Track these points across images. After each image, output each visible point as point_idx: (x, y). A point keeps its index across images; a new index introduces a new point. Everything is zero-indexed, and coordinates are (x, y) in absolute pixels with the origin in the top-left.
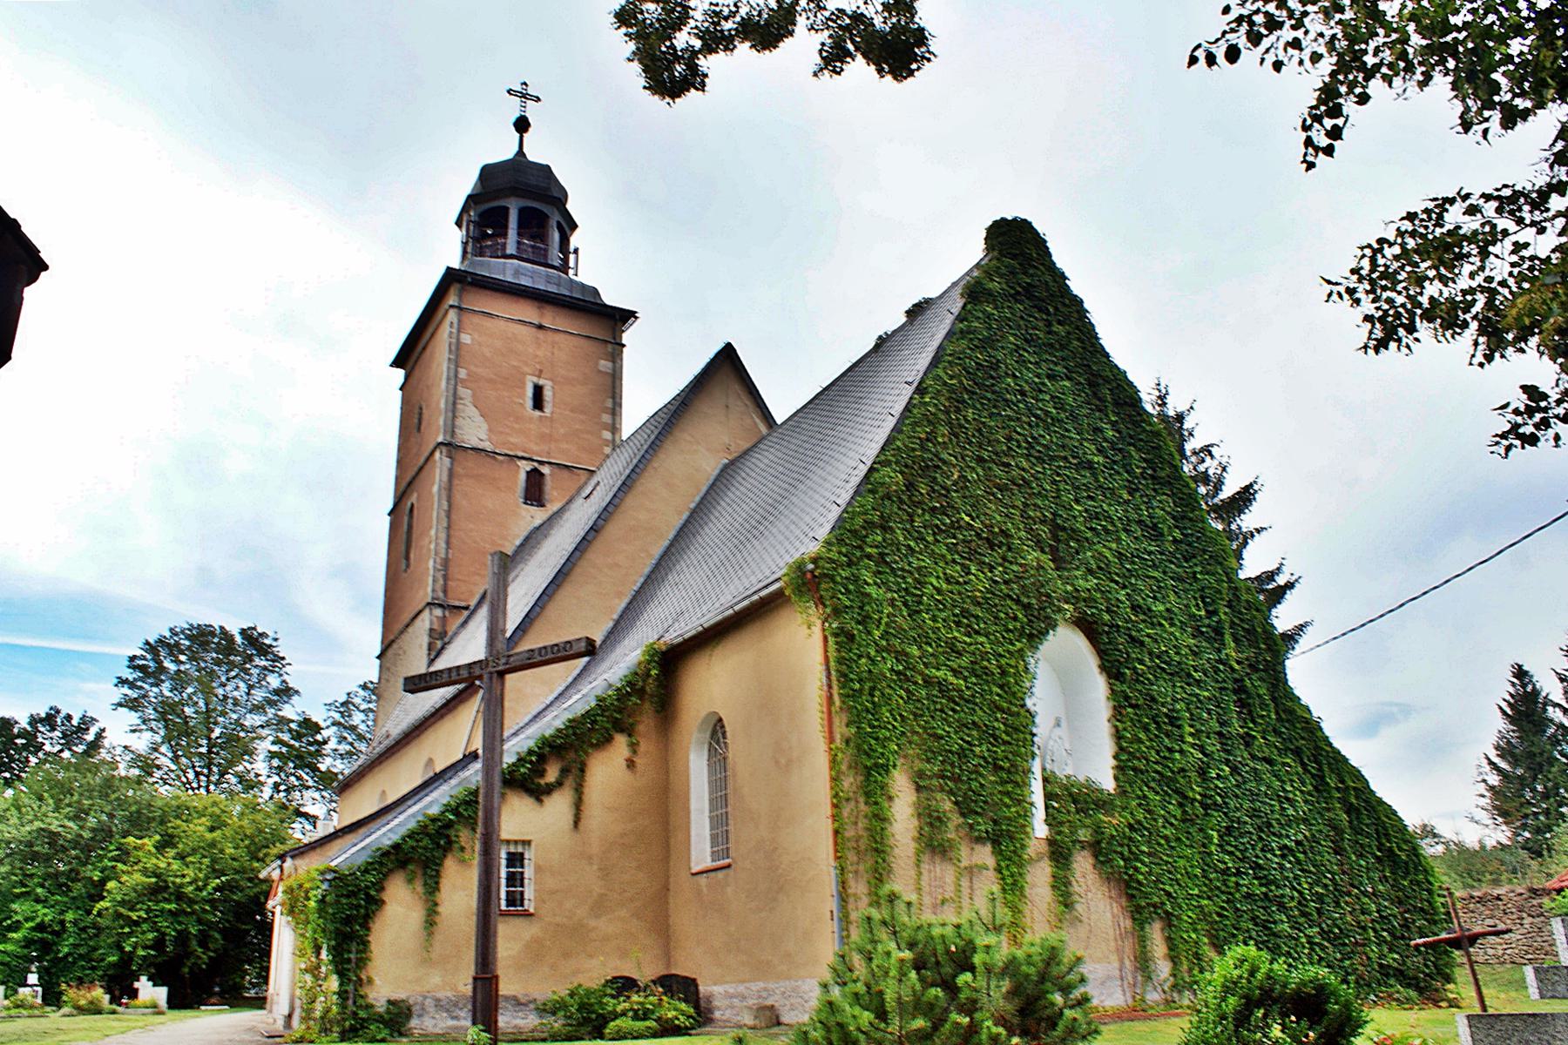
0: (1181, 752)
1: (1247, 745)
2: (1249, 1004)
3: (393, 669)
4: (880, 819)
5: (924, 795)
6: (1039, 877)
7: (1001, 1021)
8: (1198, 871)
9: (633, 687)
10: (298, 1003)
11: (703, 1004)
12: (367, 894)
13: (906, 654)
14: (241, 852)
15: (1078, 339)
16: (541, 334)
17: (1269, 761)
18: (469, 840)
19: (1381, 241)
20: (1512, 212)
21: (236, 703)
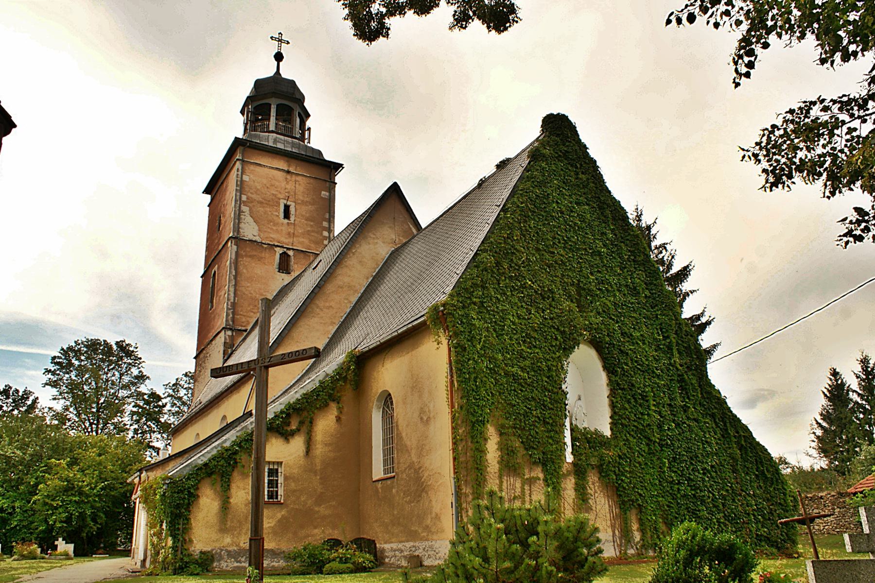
0: (648, 415)
1: (685, 411)
2: (692, 555)
3: (203, 365)
4: (481, 451)
5: (505, 437)
6: (569, 486)
7: (553, 563)
8: (657, 482)
9: (340, 375)
10: (149, 553)
11: (378, 554)
12: (189, 492)
13: (495, 359)
14: (117, 468)
15: (593, 183)
16: (289, 177)
17: (696, 420)
18: (247, 461)
19: (774, 126)
20: (848, 111)
21: (113, 383)
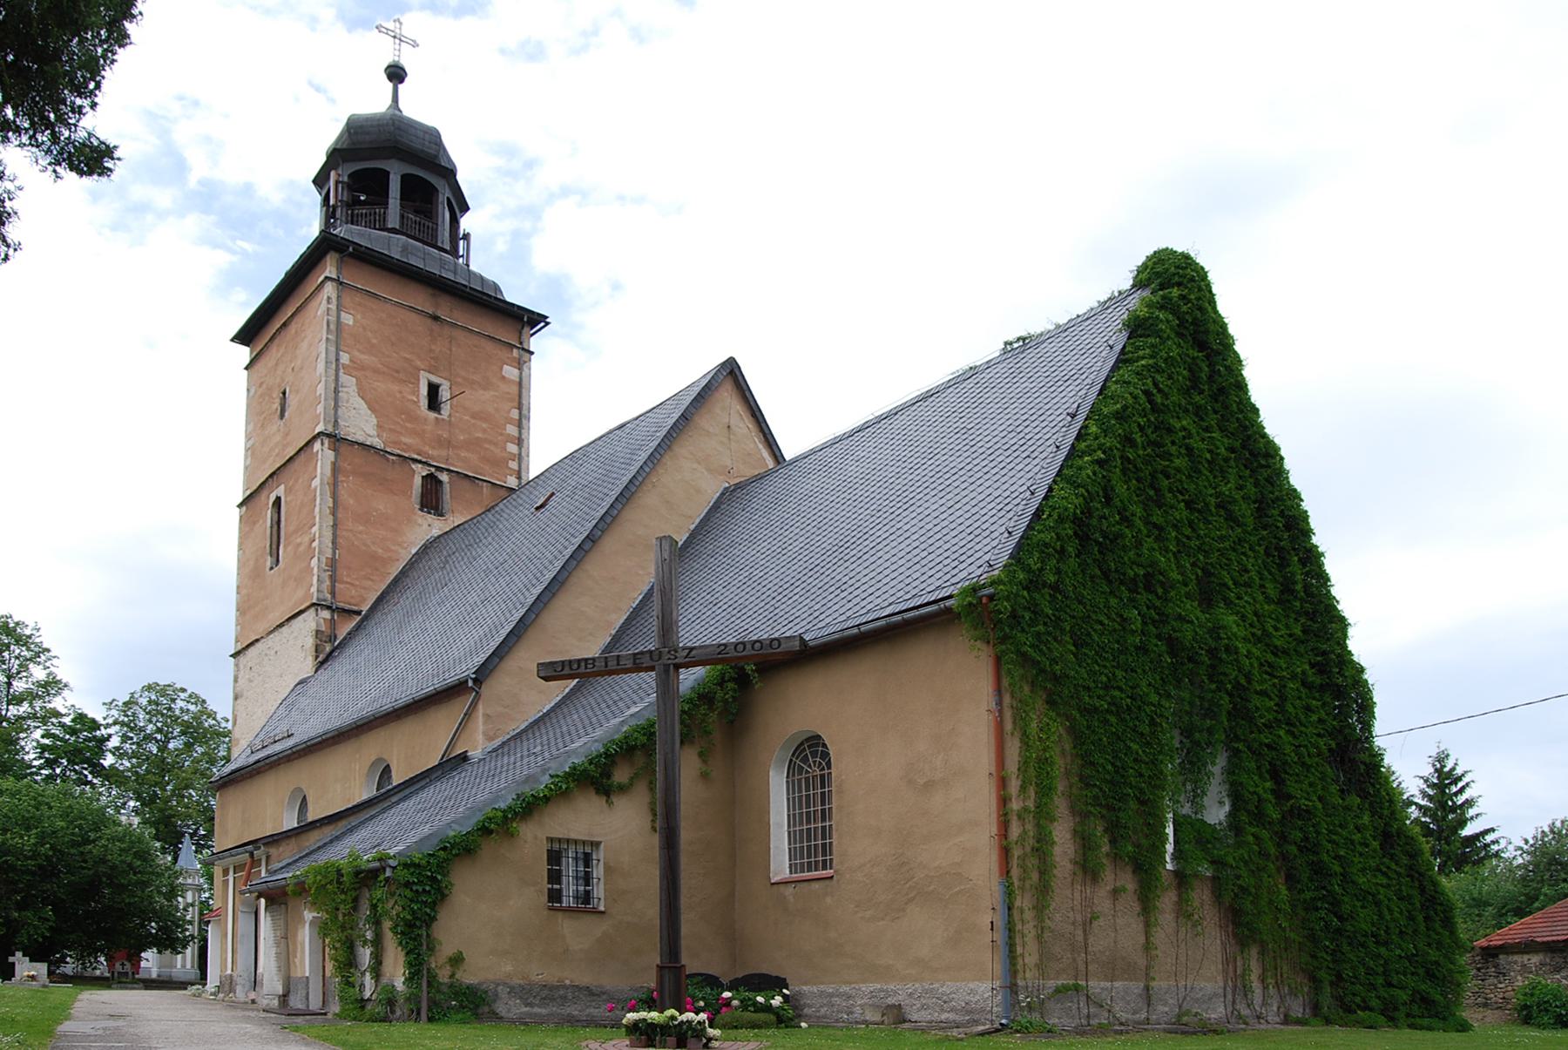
16: (435, 326)
